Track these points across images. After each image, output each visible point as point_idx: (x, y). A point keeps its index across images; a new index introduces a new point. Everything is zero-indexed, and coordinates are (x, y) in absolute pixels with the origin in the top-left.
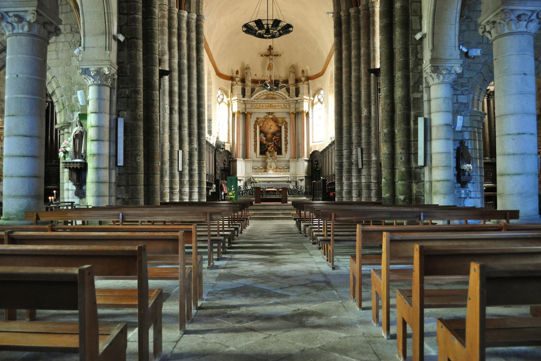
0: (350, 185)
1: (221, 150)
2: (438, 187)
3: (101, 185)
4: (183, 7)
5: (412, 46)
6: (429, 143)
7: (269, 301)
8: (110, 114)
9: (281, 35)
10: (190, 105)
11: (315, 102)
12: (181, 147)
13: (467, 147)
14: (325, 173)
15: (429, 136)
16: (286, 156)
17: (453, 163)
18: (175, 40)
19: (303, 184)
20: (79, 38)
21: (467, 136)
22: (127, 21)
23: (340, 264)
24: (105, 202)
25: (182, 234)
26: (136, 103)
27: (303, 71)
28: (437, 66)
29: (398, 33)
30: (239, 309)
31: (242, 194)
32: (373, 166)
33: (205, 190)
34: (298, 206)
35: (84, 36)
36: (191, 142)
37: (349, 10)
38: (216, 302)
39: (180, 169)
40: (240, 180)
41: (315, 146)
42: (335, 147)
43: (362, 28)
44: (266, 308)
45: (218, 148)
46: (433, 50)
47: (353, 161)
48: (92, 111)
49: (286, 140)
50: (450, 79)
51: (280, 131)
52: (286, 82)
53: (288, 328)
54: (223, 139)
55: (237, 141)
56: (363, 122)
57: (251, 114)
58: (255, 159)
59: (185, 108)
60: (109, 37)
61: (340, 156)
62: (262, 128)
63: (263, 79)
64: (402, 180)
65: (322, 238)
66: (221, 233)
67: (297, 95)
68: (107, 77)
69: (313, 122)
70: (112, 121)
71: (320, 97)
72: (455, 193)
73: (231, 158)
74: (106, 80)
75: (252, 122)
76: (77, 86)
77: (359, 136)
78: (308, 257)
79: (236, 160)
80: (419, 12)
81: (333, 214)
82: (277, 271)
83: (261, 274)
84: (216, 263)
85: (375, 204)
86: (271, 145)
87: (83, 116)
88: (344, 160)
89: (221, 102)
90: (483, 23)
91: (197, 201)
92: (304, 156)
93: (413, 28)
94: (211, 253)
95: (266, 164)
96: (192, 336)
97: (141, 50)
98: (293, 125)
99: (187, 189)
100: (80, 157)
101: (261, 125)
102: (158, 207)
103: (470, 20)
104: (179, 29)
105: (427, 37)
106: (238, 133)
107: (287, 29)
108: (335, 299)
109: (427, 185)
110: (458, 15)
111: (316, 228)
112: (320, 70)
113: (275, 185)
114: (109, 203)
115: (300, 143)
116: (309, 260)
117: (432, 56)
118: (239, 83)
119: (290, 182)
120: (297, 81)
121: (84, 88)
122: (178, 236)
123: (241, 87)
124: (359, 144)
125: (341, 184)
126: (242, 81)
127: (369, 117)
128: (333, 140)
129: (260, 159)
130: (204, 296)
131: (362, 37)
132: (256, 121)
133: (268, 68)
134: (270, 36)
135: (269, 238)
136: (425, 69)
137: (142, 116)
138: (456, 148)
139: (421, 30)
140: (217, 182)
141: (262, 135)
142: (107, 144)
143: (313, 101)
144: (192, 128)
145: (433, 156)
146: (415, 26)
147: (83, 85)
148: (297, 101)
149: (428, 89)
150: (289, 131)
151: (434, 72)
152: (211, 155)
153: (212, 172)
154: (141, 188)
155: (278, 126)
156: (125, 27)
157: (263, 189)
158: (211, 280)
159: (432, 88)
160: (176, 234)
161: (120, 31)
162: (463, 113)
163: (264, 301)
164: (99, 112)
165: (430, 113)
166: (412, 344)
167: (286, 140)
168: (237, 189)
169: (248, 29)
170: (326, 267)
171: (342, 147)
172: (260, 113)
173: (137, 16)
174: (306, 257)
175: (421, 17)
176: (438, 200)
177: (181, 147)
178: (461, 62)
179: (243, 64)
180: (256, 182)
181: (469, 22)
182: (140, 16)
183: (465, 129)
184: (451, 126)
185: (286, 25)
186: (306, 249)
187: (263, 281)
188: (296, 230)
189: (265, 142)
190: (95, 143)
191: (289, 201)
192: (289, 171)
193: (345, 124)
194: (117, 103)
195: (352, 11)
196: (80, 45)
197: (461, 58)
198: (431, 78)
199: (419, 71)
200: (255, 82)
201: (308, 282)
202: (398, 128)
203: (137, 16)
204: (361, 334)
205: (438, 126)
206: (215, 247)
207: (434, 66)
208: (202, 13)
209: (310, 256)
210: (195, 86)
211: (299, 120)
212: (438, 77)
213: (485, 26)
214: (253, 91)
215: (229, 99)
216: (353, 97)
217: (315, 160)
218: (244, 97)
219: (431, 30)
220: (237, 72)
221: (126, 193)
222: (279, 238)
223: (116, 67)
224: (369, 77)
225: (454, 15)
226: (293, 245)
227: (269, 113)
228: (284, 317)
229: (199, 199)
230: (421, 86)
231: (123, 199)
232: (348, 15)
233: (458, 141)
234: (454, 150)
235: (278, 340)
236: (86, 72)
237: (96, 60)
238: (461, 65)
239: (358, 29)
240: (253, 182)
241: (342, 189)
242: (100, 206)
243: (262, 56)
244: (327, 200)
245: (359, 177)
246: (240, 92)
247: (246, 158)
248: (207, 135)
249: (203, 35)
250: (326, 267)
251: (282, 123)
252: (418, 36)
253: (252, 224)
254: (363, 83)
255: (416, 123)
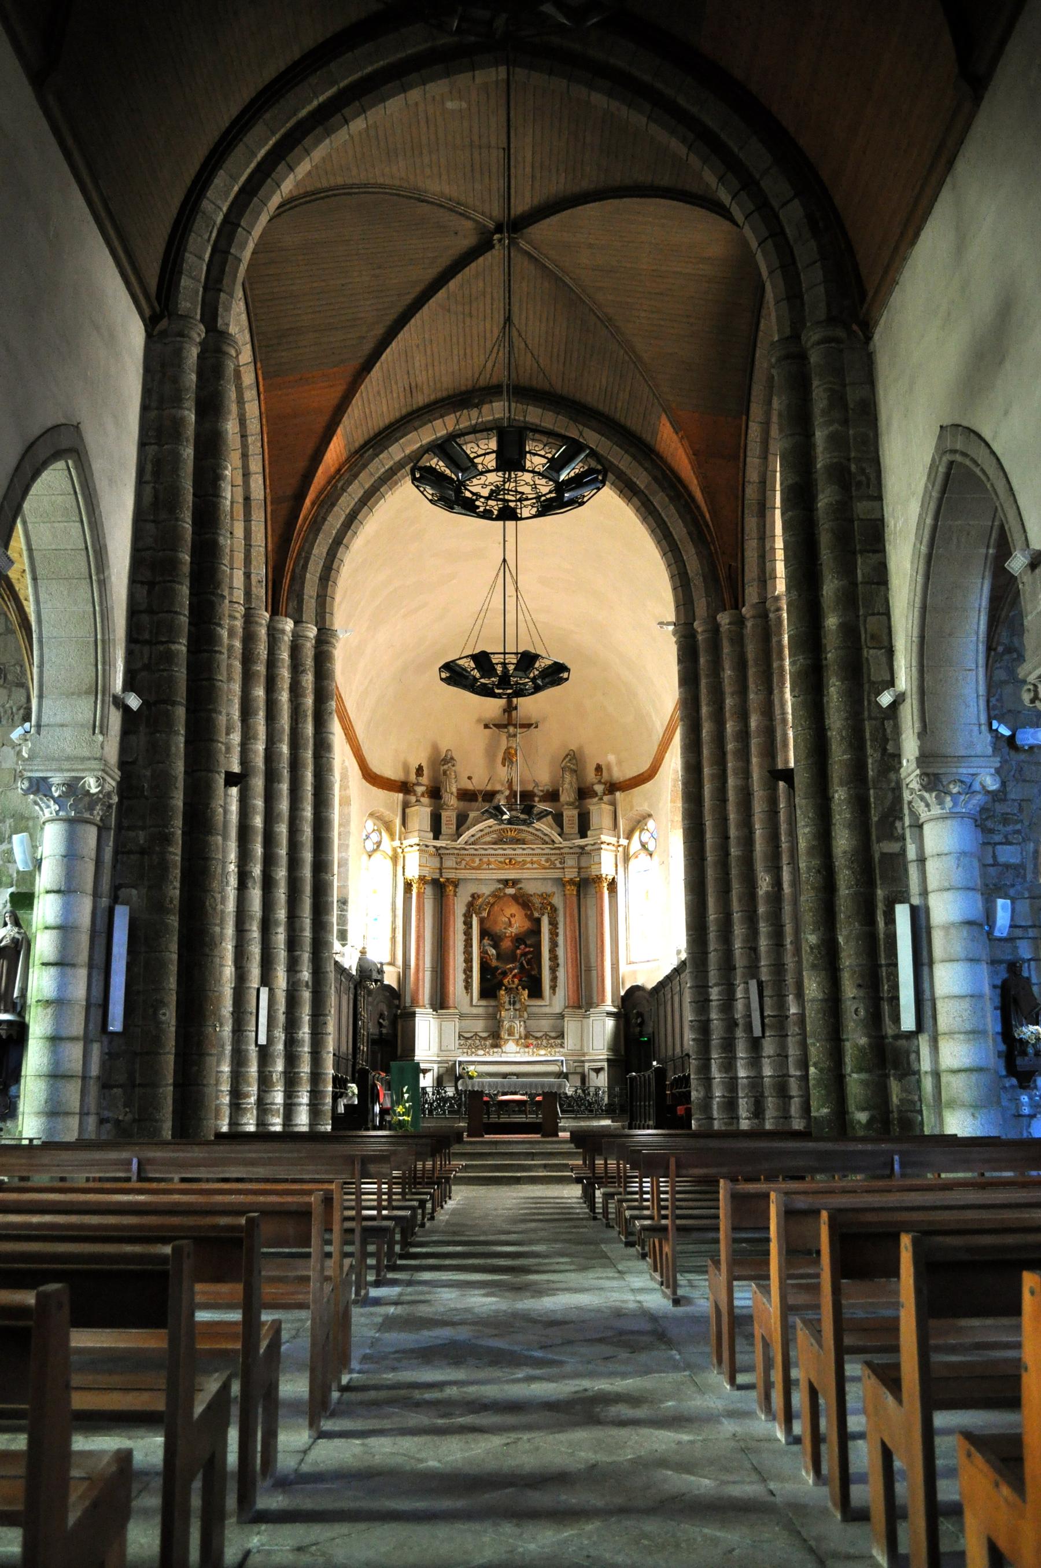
0: (732, 1084)
1: (373, 986)
2: (956, 1086)
3: (60, 1083)
4: (282, 607)
5: (874, 722)
6: (926, 969)
7: (514, 1374)
8: (96, 895)
9: (537, 689)
10: (294, 863)
11: (632, 851)
12: (266, 979)
13: (1028, 979)
14: (663, 1051)
15: (925, 953)
16: (555, 1001)
17: (992, 1023)
18: (259, 692)
19: (601, 1081)
20: (24, 700)
21: (1025, 950)
22: (150, 658)
23: (695, 1294)
24: (70, 1130)
25: (320, 1199)
26: (163, 867)
27: (599, 769)
28: (935, 775)
29: (834, 690)
30: (441, 1391)
31: (431, 1112)
32: (793, 1029)
33: (329, 1100)
34: (581, 1139)
35: (41, 697)
36: (293, 967)
37: (715, 618)
38: (385, 1376)
39: (262, 1040)
40: (425, 1071)
41: (634, 973)
42: (687, 980)
43: (751, 663)
44: (506, 1387)
45: (366, 974)
46: (923, 734)
47: (738, 1016)
48: (49, 888)
49: (554, 958)
50: (970, 806)
51: (536, 932)
52: (553, 796)
53: (561, 1427)
54: (379, 954)
55: (417, 959)
56: (762, 909)
57: (456, 884)
58: (466, 1009)
59: (281, 874)
60: (103, 701)
61: (702, 1004)
62: (487, 925)
63: (489, 788)
64: (860, 1070)
65: (647, 1222)
66: (385, 1212)
67: (583, 834)
68: (91, 801)
69: (627, 906)
70: (99, 914)
71: (645, 837)
72: (1005, 1103)
73: (398, 1007)
74: (91, 808)
75: (459, 907)
76: (9, 822)
77: (752, 949)
78: (613, 1278)
79: (414, 1014)
80: (885, 638)
81: (673, 1161)
82: (529, 1310)
83: (489, 1316)
84: (374, 1292)
85: (803, 1135)
86: (512, 972)
87: (23, 901)
88: (714, 1015)
89: (374, 851)
90: (1032, 678)
91: (305, 1129)
92: (603, 1001)
93: (873, 679)
94: (360, 1269)
95: (499, 1023)
96: (338, 1442)
97: (182, 732)
98: (572, 916)
99: (278, 1097)
100: (9, 1005)
101: (485, 914)
102: (209, 1143)
103: (1015, 656)
104: (272, 663)
105: (908, 701)
106: (420, 937)
107: (556, 674)
108: (676, 1367)
109: (928, 1084)
110: (982, 648)
111: (635, 1200)
112: (644, 766)
113: (524, 1085)
114: (80, 1132)
115: (593, 964)
116: (615, 1284)
117: (921, 748)
118: (425, 800)
119: (566, 1076)
120: (584, 793)
121: (25, 823)
122: (310, 1204)
123: (428, 810)
124: (753, 970)
125: (707, 1081)
126: (431, 792)
127: (776, 897)
128: (684, 956)
129: (480, 1011)
130: (355, 1364)
131: (752, 686)
132: (470, 905)
133: (504, 759)
134: (510, 691)
135: (509, 1233)
136: (908, 780)
137: (176, 902)
138: (999, 982)
139: (891, 683)
140: (361, 1078)
141: (486, 941)
142: (83, 973)
143: (626, 849)
144: (297, 926)
145: (940, 1005)
146: (877, 674)
147: (28, 819)
148: (582, 848)
149: (917, 830)
150: (561, 931)
151: (926, 788)
152: (345, 998)
153: (346, 1047)
154: (167, 1091)
155: (530, 917)
156: (144, 674)
157: (489, 1095)
158: (365, 1329)
159: (926, 827)
160: (306, 1199)
161: (130, 685)
162: (1012, 892)
163: (501, 1374)
164: (66, 891)
165: (925, 893)
166: (913, 1535)
167: (554, 958)
168: (418, 1094)
169: (454, 675)
170: (657, 1301)
171: (706, 978)
172: (482, 879)
173: (174, 647)
174: (608, 1278)
175: (890, 652)
176: (958, 1124)
177: (266, 979)
178: (996, 762)
179: (435, 749)
180: (471, 1078)
181: (1014, 660)
182: (181, 647)
183: (1018, 932)
184: (980, 925)
185: (550, 666)
186: (608, 1258)
187: (496, 1332)
188: (584, 1210)
189: (494, 963)
190: (52, 970)
191: (564, 1130)
192: (562, 1046)
193: (712, 915)
194: (114, 867)
195: (724, 619)
196: (27, 718)
197: (996, 749)
198: (923, 804)
199: (893, 785)
200: (467, 796)
201: (610, 1333)
202: (845, 932)
203: (174, 647)
204: (728, 1435)
205: (947, 928)
206: (371, 1255)
207: (927, 775)
208: (332, 624)
209: (616, 1275)
210: (308, 813)
211: (590, 902)
212: (941, 803)
213: (1035, 686)
214: (462, 820)
215: (397, 843)
216: (733, 841)
217: (636, 1010)
218: (436, 837)
219: (915, 683)
220: (419, 771)
221: (125, 1106)
222: (534, 1230)
223: (117, 774)
224: (774, 789)
225: (972, 647)
226: (574, 1248)
227: (506, 882)
228: (551, 1406)
229: (311, 1125)
230: (898, 824)
231: (118, 1123)
232: (715, 629)
233: (1004, 966)
234: (995, 987)
235: (537, 1449)
236: (39, 787)
237: (68, 759)
238: (998, 771)
239: (741, 666)
240: (461, 1077)
241: (709, 1097)
242: (57, 1139)
243: (486, 726)
244: (668, 1129)
245: (755, 1062)
246: (427, 824)
247: (442, 1008)
248: (337, 946)
249: (333, 679)
250: (657, 1301)
251: (543, 908)
252: (886, 699)
253: (459, 1197)
254: (759, 807)
255: (890, 920)
